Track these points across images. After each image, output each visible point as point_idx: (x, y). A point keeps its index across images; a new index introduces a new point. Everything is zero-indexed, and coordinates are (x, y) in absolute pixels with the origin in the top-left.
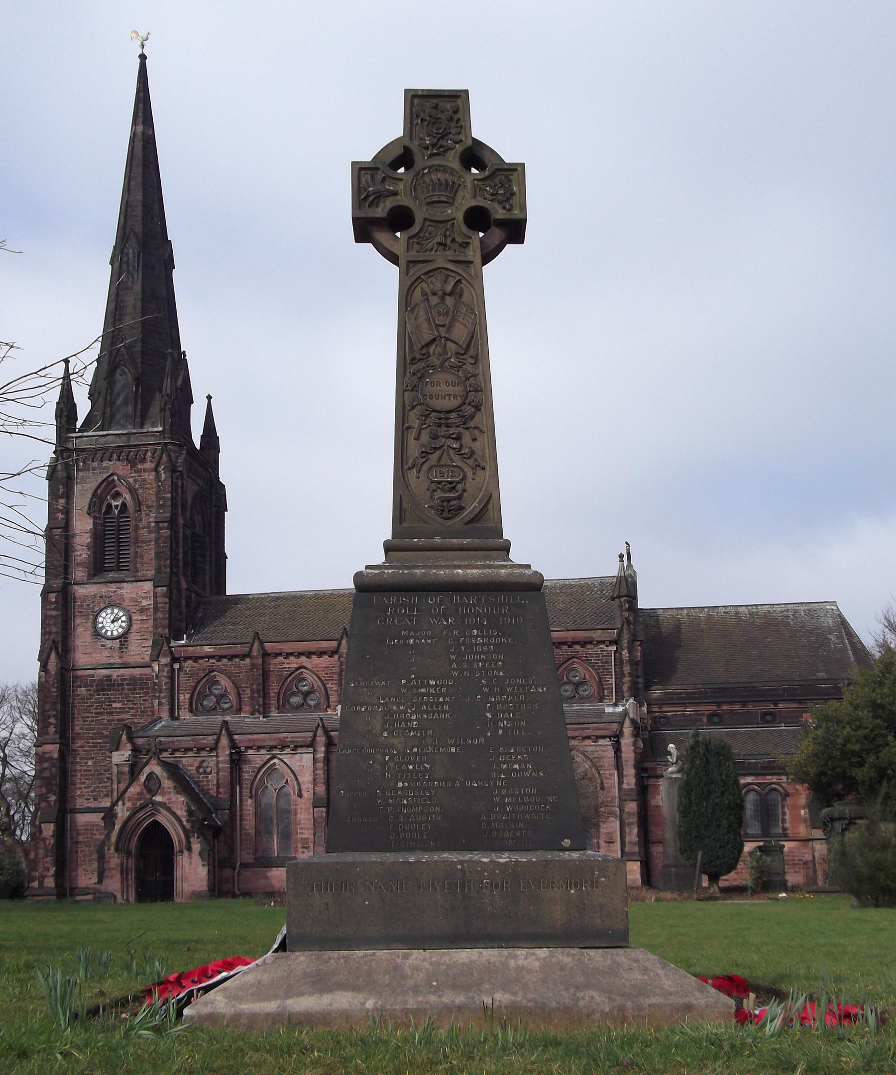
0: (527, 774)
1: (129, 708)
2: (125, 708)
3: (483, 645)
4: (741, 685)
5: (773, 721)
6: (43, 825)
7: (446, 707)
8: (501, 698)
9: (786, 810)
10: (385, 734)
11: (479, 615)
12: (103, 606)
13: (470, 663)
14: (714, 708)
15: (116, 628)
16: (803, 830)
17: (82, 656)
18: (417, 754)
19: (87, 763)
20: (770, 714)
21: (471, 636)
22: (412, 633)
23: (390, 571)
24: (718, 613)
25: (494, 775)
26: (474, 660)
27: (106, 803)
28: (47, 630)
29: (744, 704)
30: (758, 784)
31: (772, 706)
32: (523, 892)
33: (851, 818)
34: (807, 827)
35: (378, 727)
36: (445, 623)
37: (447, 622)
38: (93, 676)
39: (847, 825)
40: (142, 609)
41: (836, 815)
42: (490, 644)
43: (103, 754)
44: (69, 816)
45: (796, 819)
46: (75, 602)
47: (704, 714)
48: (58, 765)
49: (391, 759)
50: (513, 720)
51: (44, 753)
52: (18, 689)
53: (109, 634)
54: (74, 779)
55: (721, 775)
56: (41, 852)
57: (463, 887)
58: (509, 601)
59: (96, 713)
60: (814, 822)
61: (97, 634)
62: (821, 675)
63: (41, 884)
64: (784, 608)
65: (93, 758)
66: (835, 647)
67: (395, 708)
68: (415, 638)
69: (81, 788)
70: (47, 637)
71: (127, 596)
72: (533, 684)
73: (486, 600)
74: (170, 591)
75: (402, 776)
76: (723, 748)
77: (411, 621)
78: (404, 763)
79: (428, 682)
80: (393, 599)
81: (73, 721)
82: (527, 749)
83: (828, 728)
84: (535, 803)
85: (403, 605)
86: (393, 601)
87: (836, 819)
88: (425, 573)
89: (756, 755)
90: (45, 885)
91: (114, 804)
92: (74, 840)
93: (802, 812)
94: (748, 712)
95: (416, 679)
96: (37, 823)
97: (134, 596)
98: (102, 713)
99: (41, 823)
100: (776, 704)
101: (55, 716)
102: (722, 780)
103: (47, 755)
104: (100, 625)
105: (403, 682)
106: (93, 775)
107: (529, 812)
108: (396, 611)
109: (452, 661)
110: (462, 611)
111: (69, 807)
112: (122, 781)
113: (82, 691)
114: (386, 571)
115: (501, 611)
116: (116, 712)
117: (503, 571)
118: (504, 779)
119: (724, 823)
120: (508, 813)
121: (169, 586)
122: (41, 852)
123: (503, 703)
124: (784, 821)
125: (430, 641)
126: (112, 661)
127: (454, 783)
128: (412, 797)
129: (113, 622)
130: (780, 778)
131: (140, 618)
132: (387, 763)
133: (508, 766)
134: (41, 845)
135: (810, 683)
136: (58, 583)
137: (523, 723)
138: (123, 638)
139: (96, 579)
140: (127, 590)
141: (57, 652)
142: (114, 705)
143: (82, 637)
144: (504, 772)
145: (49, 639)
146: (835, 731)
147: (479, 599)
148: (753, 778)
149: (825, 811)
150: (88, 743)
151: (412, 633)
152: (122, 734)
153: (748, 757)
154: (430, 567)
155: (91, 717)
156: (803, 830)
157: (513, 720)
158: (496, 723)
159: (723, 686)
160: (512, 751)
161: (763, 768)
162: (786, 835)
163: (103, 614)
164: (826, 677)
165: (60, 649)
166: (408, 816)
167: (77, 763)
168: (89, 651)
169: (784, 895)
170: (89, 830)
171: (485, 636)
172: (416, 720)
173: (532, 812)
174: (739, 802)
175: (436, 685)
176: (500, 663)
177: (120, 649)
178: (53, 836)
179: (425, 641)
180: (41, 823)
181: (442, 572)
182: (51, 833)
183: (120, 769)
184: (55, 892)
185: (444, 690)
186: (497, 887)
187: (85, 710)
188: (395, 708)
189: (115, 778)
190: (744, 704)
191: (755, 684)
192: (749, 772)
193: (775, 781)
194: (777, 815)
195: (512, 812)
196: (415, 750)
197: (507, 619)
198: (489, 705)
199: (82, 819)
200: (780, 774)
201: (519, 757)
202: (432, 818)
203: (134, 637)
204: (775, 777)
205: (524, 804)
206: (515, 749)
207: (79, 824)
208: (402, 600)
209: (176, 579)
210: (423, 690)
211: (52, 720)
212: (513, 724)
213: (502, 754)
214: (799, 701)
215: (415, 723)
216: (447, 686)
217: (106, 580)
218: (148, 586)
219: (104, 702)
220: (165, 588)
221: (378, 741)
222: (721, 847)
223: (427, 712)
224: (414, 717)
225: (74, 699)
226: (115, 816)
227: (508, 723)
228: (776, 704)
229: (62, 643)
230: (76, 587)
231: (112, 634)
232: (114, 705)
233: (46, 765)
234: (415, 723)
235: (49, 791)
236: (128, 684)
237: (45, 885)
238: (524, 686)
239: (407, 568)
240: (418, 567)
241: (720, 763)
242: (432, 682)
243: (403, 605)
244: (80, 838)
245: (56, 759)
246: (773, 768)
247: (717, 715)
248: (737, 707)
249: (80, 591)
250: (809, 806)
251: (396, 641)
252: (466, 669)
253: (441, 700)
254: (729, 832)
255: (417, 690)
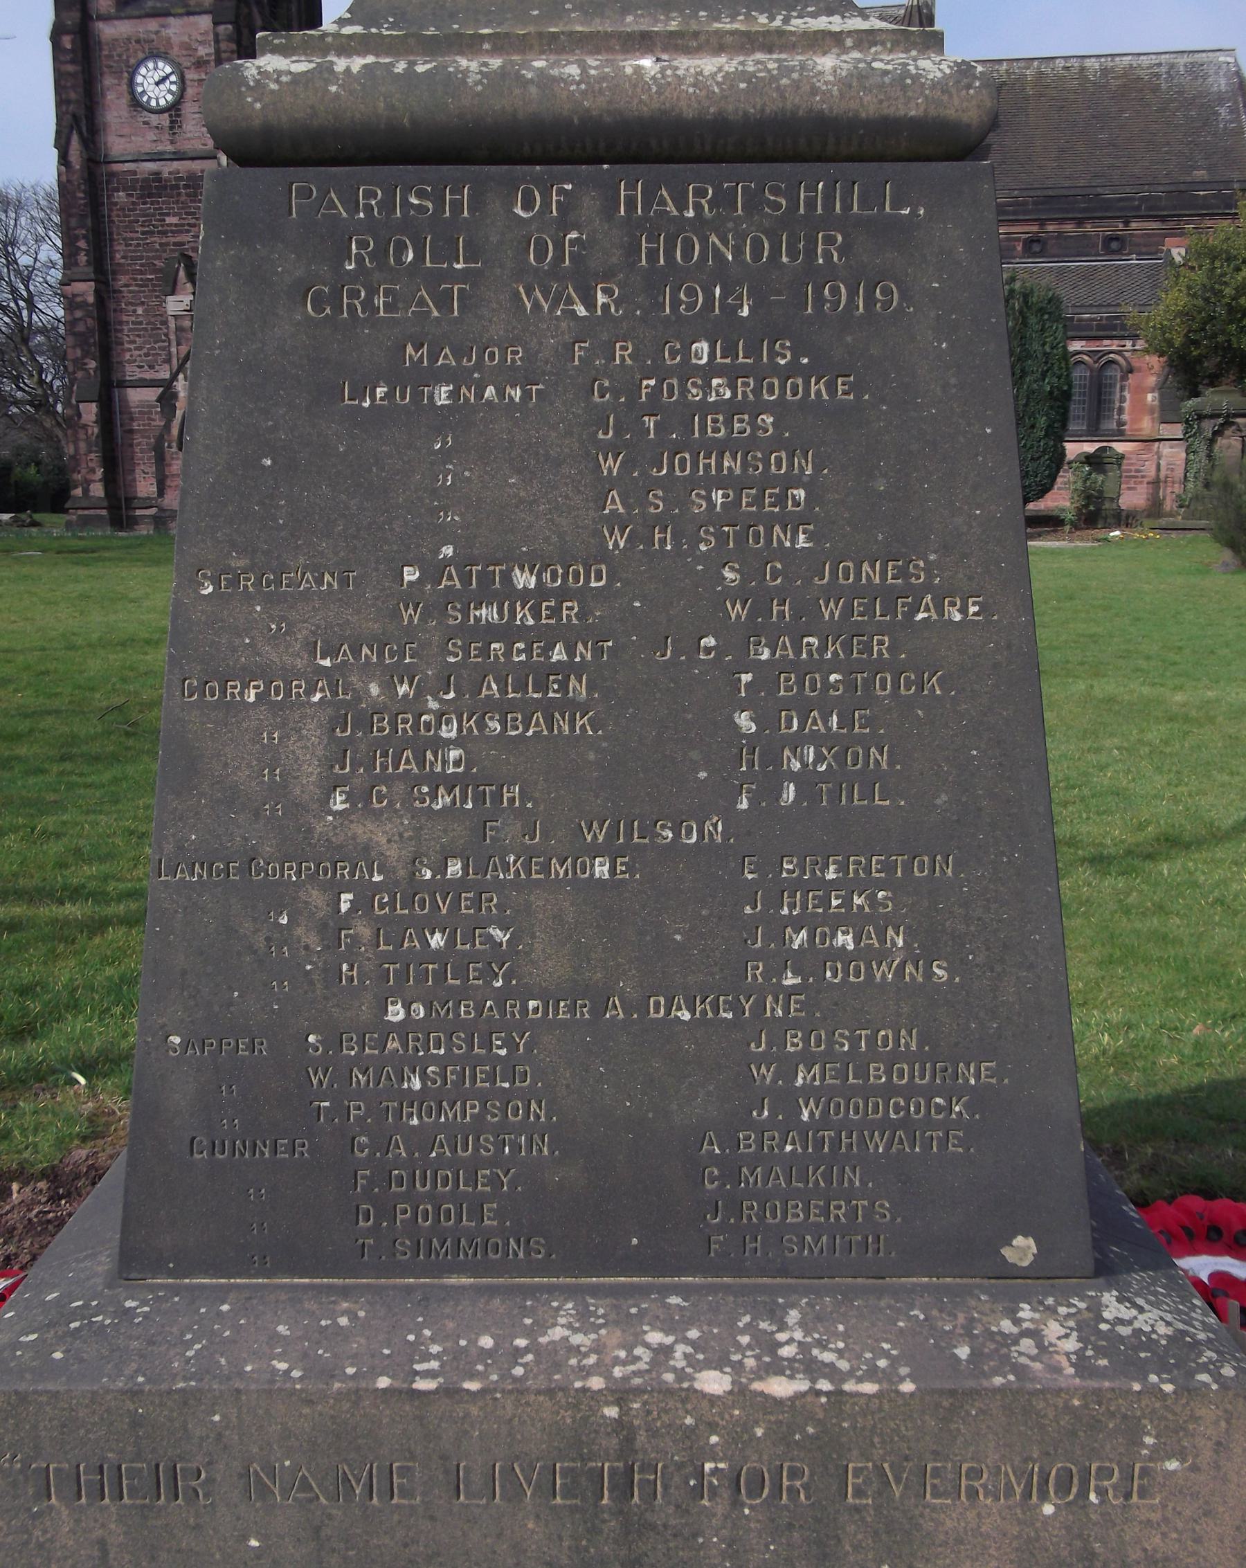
0: (884, 973)
1: (189, 225)
2: (183, 225)
3: (731, 409)
4: (1079, 191)
5: (1118, 252)
6: (81, 406)
7: (578, 688)
8: (798, 652)
9: (1127, 394)
10: (339, 803)
11: (721, 273)
12: (141, 55)
13: (677, 490)
14: (1035, 229)
15: (162, 94)
16: (1147, 426)
17: (118, 140)
18: (460, 885)
19: (135, 311)
20: (1117, 239)
21: (687, 371)
22: (446, 358)
23: (357, 63)
24: (1053, 69)
25: (756, 972)
26: (692, 482)
27: (165, 374)
28: (64, 96)
29: (1080, 222)
30: (1089, 353)
31: (1121, 226)
32: (857, 1509)
33: (1228, 416)
34: (1153, 419)
35: (311, 772)
36: (581, 311)
37: (590, 304)
38: (135, 173)
39: (1221, 425)
40: (198, 62)
41: (1207, 411)
42: (757, 409)
43: (157, 297)
44: (116, 390)
45: (1139, 407)
46: (101, 50)
47: (1018, 240)
48: (95, 314)
49: (363, 904)
50: (838, 744)
51: (74, 296)
52: (39, 189)
53: (153, 103)
54: (119, 335)
55: (1044, 344)
56: (82, 445)
57: (624, 1484)
58: (847, 207)
59: (143, 233)
60: (1167, 413)
61: (136, 104)
62: (1200, 174)
63: (86, 491)
64: (1154, 60)
65: (143, 303)
66: (1225, 128)
67: (374, 689)
68: (456, 378)
69: (130, 350)
70: (64, 108)
71: (175, 40)
72: (927, 587)
73: (754, 203)
74: (238, 30)
75: (403, 976)
76: (1050, 301)
77: (443, 301)
78: (412, 921)
79: (507, 577)
80: (369, 195)
81: (111, 246)
82: (889, 868)
83: (1213, 270)
84: (909, 1092)
85: (412, 228)
86: (368, 209)
87: (1206, 417)
88: (502, 73)
89: (1091, 305)
90: (92, 494)
91: (174, 377)
92: (128, 428)
93: (1150, 397)
94: (1085, 236)
95: (462, 562)
96: (74, 402)
97: (186, 39)
98: (152, 233)
99: (78, 402)
100: (1127, 223)
101: (85, 237)
102: (1045, 354)
103: (79, 299)
104: (140, 89)
105: (411, 575)
106: (146, 329)
107: (885, 1125)
108: (380, 255)
109: (603, 486)
110: (653, 255)
111: (115, 377)
112: (183, 341)
113: (121, 196)
114: (340, 64)
115: (811, 253)
116: (172, 232)
117: (827, 63)
118: (794, 990)
119: (1042, 421)
120: (804, 1130)
121: (235, 23)
122: (82, 445)
123: (802, 670)
124: (1121, 410)
125: (517, 394)
126: (160, 148)
127: (599, 1010)
128: (443, 1063)
129: (157, 84)
130: (1122, 343)
131: (196, 77)
132: (344, 922)
133: (812, 936)
134: (82, 435)
135: (1182, 187)
136: (72, 18)
137: (880, 758)
138: (174, 109)
139: (129, 11)
140: (176, 29)
141: (80, 133)
142: (169, 220)
143: (114, 112)
144: (799, 961)
145: (67, 113)
146: (1224, 275)
147: (724, 200)
148: (1083, 343)
149: (1191, 403)
150: (135, 280)
151: (446, 358)
152: (178, 270)
153: (1078, 310)
154: (524, 45)
155: (138, 239)
156: (1147, 426)
157: (838, 744)
158: (773, 759)
159: (1050, 193)
160: (831, 875)
161: (1100, 327)
162: (1121, 433)
163: (143, 71)
164: (1206, 178)
165: (84, 129)
166: (422, 1140)
167: (121, 311)
168: (126, 131)
169: (1117, 533)
170: (144, 413)
171: (744, 372)
172: (457, 743)
173: (894, 1126)
174: (1065, 388)
175: (541, 592)
176: (801, 494)
177: (171, 128)
178: (95, 422)
179: (501, 393)
180: (78, 402)
181: (573, 70)
182: (93, 418)
183: (180, 322)
184: (105, 504)
185: (570, 610)
186: (755, 1491)
187: (126, 227)
188: (374, 689)
189: (173, 337)
190: (1080, 222)
191: (1100, 190)
192: (1079, 334)
193: (1114, 348)
194: (1111, 402)
195: (824, 1122)
196: (455, 868)
197: (835, 291)
198: (746, 678)
199: (137, 396)
200: (1123, 338)
201: (858, 901)
202: (516, 1148)
203: (189, 108)
204: (1116, 342)
205: (866, 1092)
206: (843, 868)
207: (132, 405)
208: (405, 203)
209: (246, 10)
210: (488, 613)
211: (82, 244)
212: (841, 758)
213: (796, 885)
214: (1162, 219)
215: (454, 754)
216: (583, 595)
217: (143, 12)
218: (205, 22)
219: (154, 215)
220: (230, 27)
221: (310, 830)
222: (1032, 459)
223: (503, 709)
224: (449, 732)
225: (110, 210)
226: (175, 396)
227: (819, 758)
228: (1127, 223)
229: (86, 117)
230: (101, 25)
231: (158, 103)
232: (169, 220)
233: (79, 314)
234: (454, 754)
235: (86, 354)
236: (186, 187)
237: (92, 494)
238: (890, 597)
239: (432, 47)
240: (471, 45)
241: (1043, 326)
242: (524, 580)
243: (412, 228)
244: (135, 426)
245: (92, 305)
246: (1114, 328)
247: (1038, 241)
248: (1069, 227)
249: (109, 31)
250: (1161, 387)
251: (379, 392)
252: (661, 522)
253: (558, 654)
254: (1046, 435)
255: (466, 613)
